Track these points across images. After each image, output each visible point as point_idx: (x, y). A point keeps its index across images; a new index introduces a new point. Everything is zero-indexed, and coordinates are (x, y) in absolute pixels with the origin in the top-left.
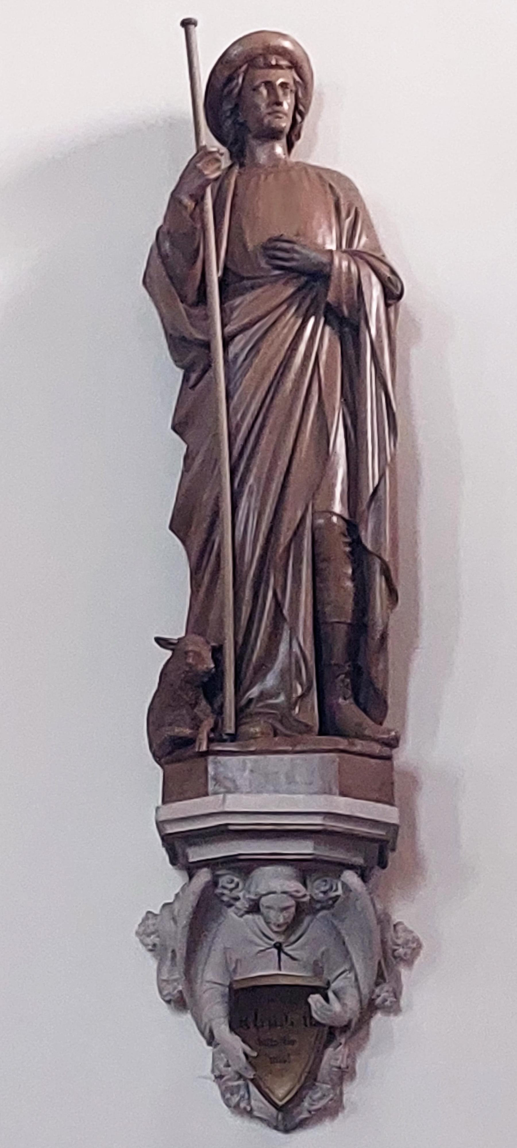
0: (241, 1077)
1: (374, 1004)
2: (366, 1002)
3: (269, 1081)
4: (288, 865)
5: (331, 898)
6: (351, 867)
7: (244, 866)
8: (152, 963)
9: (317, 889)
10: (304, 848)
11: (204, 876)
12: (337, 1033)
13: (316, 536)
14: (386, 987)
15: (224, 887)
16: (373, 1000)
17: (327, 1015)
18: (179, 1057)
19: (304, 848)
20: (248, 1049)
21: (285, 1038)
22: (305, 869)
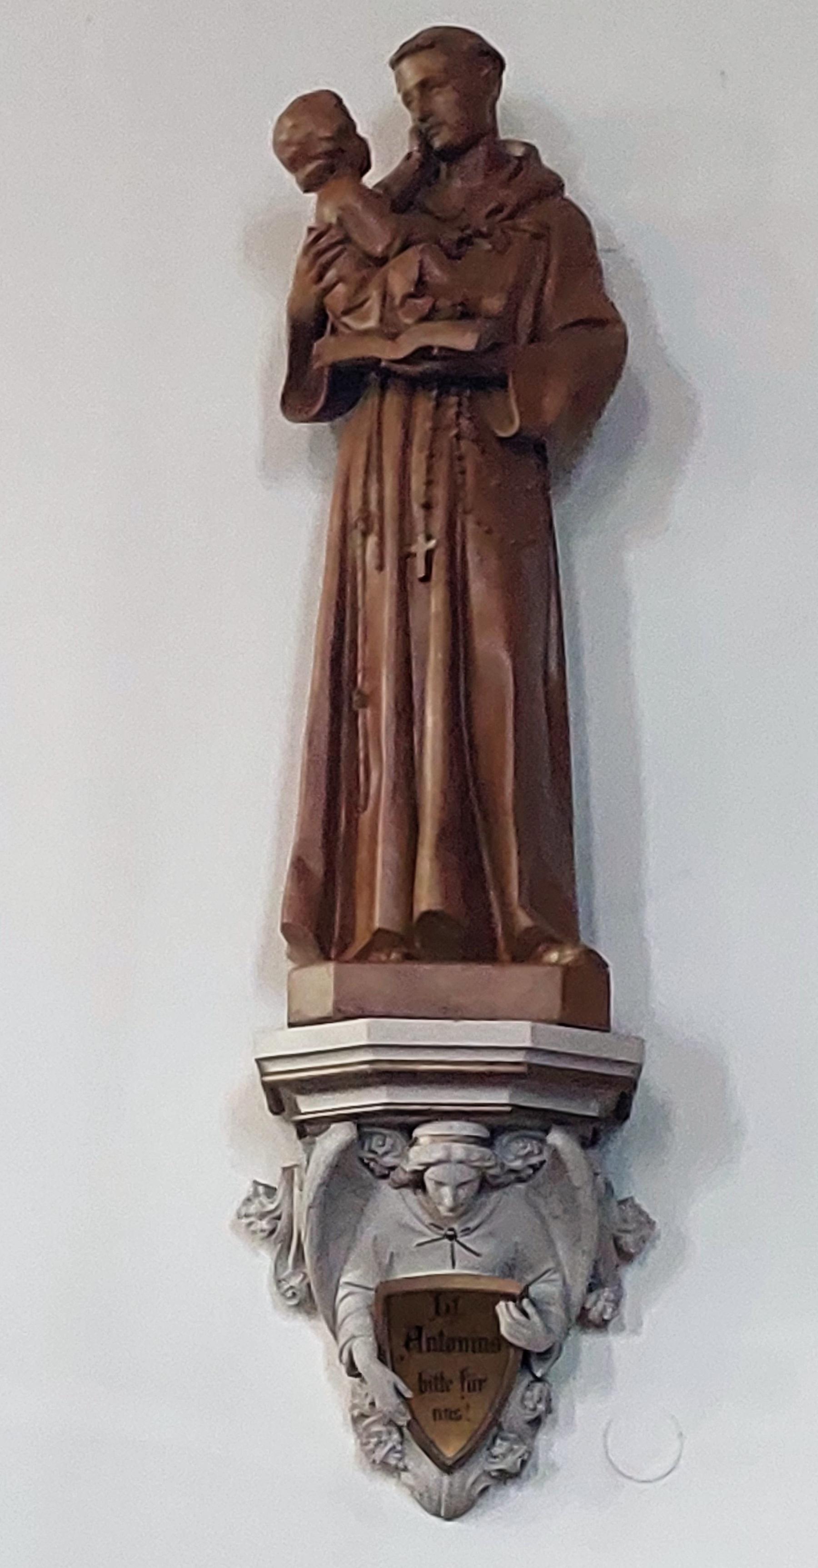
0: (391, 1422)
1: (587, 1316)
2: (576, 1311)
3: (433, 1429)
4: (468, 1121)
5: (531, 1166)
6: (562, 1120)
7: (405, 1123)
8: (264, 1259)
9: (515, 1153)
10: (498, 1097)
11: (338, 1136)
12: (540, 1145)
13: (543, 1018)
14: (607, 1293)
15: (371, 1151)
16: (412, 234)
17: (523, 1334)
18: (309, 1378)
19: (498, 1097)
20: (402, 1386)
21: (458, 1378)
22: (495, 1127)
